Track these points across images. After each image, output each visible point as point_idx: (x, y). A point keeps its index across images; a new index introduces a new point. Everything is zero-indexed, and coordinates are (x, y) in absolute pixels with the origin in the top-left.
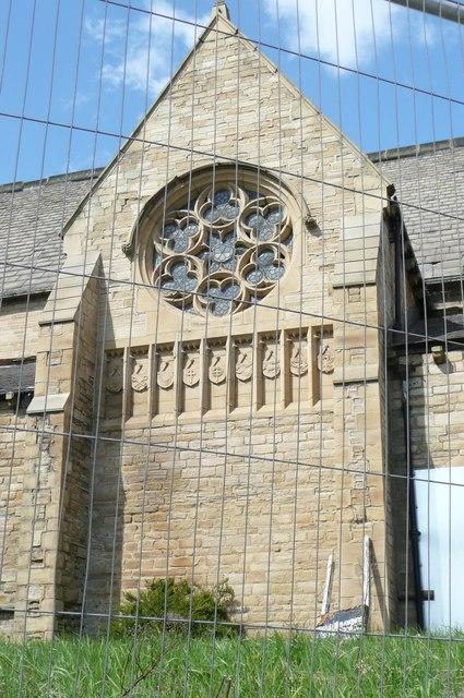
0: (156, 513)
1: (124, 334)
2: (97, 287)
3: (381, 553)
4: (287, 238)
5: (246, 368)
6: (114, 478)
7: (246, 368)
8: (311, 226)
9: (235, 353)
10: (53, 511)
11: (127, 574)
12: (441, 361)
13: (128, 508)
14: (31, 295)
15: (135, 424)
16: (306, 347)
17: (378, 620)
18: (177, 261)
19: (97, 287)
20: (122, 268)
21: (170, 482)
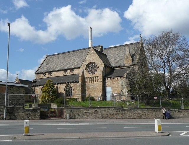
0: (88, 90)
1: (86, 76)
2: (83, 72)
3: (102, 94)
4: (97, 68)
5: (96, 79)
6: (85, 88)
7: (96, 79)
8: (99, 68)
9: (88, 79)
10: (81, 91)
11: (87, 95)
12: (107, 79)
13: (87, 90)
14: (4, 119)
15: (86, 84)
16: (95, 78)
17: (101, 99)
18: (89, 70)
19: (83, 72)
20: (85, 71)
21: (89, 88)
